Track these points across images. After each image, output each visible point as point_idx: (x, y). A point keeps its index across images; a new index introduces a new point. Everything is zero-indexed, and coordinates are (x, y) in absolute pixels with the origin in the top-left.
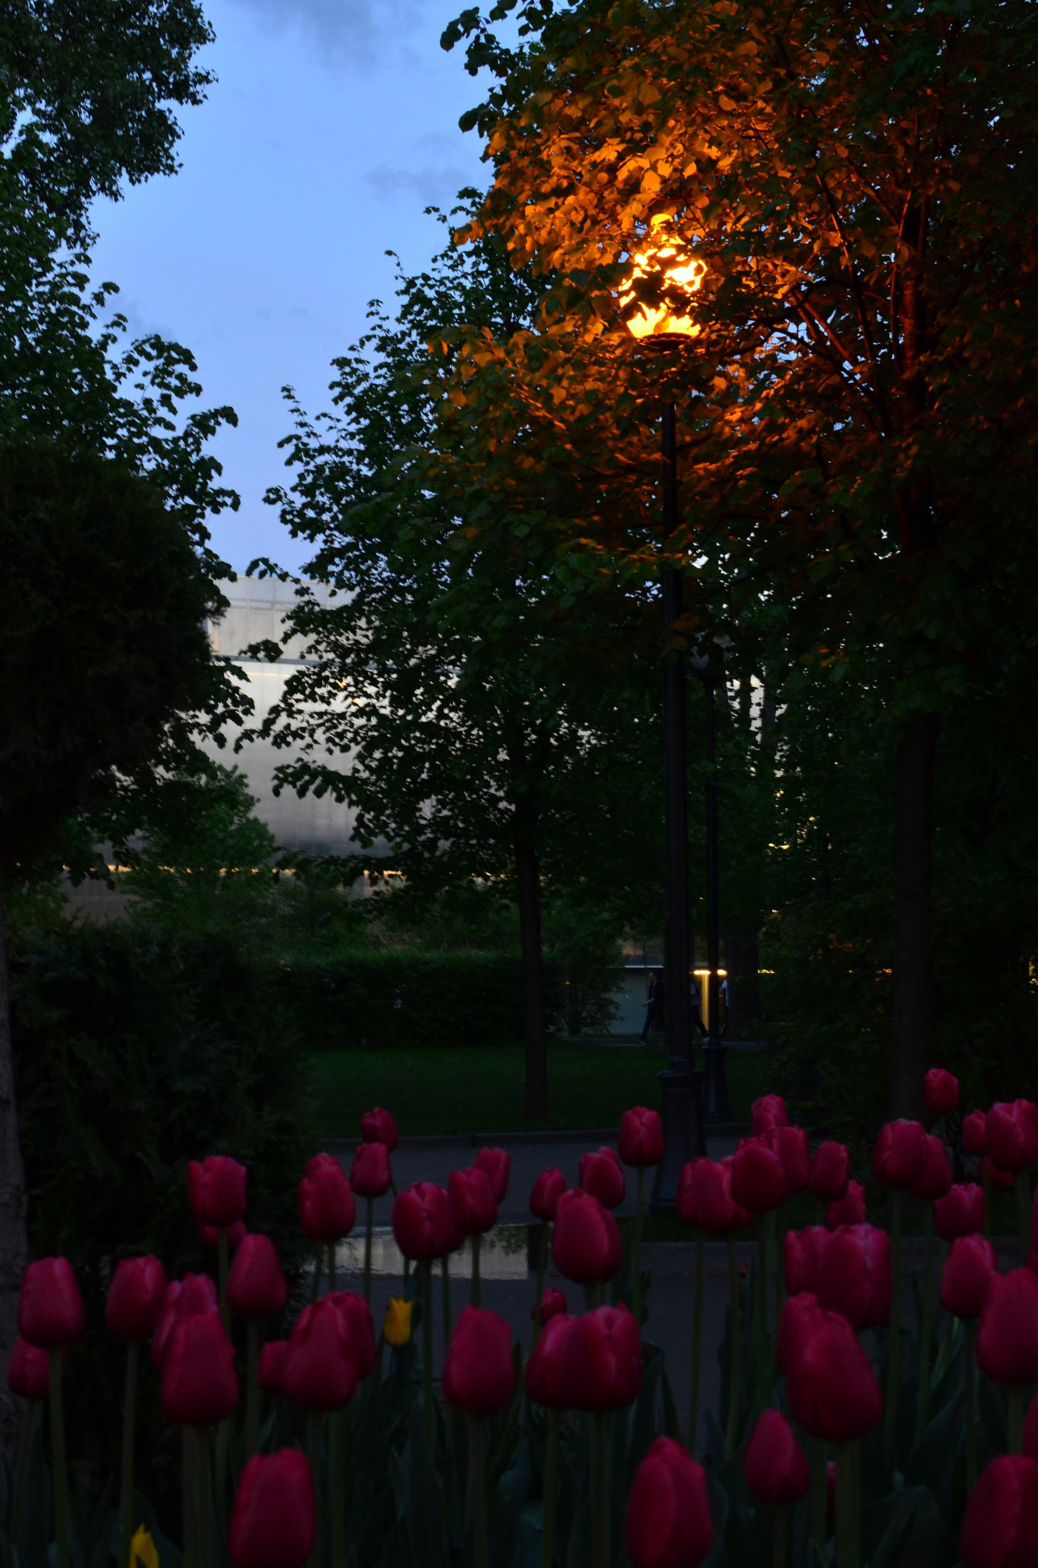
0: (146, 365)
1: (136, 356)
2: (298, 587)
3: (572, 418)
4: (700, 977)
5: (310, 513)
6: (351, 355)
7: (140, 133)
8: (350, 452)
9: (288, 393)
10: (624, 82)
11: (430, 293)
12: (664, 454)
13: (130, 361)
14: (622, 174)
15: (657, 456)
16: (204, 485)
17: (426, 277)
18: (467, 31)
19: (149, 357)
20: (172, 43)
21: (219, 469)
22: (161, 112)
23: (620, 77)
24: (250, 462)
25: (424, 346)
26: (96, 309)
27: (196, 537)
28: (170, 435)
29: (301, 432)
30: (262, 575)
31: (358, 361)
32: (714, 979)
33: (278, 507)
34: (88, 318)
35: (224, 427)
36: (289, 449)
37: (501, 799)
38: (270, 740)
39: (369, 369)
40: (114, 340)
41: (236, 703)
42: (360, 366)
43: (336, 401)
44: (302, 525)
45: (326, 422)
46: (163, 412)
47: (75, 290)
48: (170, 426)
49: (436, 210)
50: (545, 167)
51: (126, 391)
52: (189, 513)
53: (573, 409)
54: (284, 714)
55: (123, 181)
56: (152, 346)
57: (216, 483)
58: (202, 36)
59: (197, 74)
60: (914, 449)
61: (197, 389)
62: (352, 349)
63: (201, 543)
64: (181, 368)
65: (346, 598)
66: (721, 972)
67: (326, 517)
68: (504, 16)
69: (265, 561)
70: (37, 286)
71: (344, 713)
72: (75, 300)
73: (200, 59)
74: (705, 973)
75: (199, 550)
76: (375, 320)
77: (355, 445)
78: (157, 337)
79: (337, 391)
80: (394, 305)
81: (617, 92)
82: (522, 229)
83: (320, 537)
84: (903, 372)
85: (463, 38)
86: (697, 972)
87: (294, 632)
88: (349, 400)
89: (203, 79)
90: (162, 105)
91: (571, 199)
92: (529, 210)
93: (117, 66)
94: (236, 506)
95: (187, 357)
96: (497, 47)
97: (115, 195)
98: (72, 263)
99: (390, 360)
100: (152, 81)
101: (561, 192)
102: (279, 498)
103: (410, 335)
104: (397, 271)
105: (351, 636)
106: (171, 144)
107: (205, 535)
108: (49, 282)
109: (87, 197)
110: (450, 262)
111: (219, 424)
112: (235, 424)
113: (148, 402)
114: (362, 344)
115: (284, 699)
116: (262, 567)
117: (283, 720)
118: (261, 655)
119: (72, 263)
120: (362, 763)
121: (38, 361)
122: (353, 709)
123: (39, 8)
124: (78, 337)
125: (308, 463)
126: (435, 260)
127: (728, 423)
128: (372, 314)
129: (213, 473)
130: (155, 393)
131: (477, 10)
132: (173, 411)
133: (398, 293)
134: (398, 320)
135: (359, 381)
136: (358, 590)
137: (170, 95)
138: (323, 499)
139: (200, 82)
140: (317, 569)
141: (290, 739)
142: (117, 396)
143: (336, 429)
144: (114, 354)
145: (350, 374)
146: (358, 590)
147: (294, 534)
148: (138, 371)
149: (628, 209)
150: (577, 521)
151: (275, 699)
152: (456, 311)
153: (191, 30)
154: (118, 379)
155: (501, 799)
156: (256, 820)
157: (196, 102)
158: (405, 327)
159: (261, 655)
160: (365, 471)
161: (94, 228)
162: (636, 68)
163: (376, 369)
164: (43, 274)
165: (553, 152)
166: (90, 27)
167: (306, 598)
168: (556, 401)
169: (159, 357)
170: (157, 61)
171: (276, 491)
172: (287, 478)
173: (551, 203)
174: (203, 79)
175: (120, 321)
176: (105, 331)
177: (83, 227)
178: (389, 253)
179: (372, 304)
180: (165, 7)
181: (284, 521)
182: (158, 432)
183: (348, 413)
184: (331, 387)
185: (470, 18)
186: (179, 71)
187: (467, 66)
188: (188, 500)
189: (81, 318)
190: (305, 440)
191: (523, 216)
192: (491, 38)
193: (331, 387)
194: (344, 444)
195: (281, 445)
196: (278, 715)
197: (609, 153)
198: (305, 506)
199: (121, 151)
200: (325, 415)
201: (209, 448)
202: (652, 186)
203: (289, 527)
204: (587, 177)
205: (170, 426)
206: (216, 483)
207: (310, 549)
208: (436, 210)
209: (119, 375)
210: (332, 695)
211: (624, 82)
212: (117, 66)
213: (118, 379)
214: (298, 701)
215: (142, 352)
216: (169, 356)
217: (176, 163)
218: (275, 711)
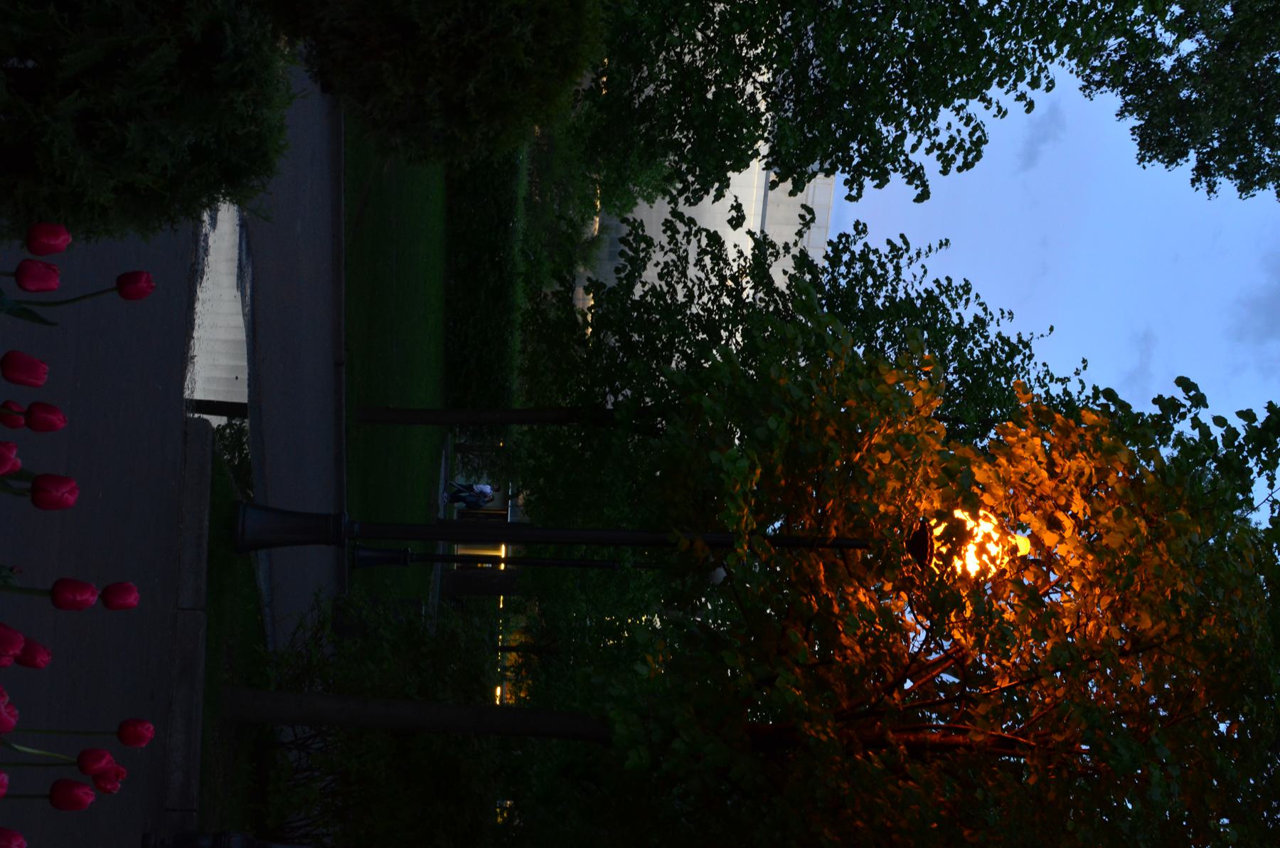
0: (966, 131)
1: (973, 124)
2: (791, 245)
3: (865, 467)
4: (498, 549)
5: (846, 257)
6: (972, 295)
7: (1171, 136)
8: (895, 290)
9: (944, 244)
10: (1125, 521)
11: (1018, 360)
12: (836, 538)
13: (969, 119)
14: (1060, 515)
15: (834, 533)
16: (867, 174)
17: (1031, 357)
18: (1190, 398)
19: (971, 135)
20: (1240, 166)
21: (879, 186)
22: (1187, 154)
23: (1129, 517)
24: (885, 211)
25: (976, 352)
26: (1013, 95)
27: (827, 166)
28: (907, 148)
29: (913, 252)
30: (802, 217)
31: (967, 301)
32: (497, 560)
33: (852, 232)
34: (1006, 87)
35: (913, 192)
36: (899, 243)
37: (616, 398)
38: (669, 217)
39: (961, 309)
40: (987, 108)
41: (695, 192)
42: (963, 302)
43: (937, 281)
44: (838, 247)
45: (920, 273)
46: (926, 143)
47: (1028, 78)
48: (914, 148)
49: (1085, 368)
50: (1070, 455)
51: (945, 115)
52: (847, 161)
53: (872, 468)
54: (687, 229)
55: (1133, 121)
56: (979, 138)
57: (868, 183)
58: (1245, 189)
59: (1215, 183)
60: (824, 738)
61: (945, 172)
62: (977, 296)
63: (821, 169)
64: (960, 160)
65: (781, 282)
66: (502, 566)
67: (843, 269)
68: (1193, 428)
69: (813, 220)
70: (1033, 49)
71: (686, 277)
72: (1021, 77)
73: (1227, 186)
74: (502, 552)
75: (816, 166)
76: (997, 315)
77: (901, 294)
78: (986, 142)
79: (945, 283)
80: (1010, 331)
81: (1118, 515)
82: (1023, 432)
83: (826, 264)
84: (893, 732)
85: (1183, 395)
86: (503, 547)
87: (755, 240)
88: (937, 291)
89: (1211, 188)
90: (1192, 155)
91: (1045, 474)
92: (1037, 441)
93: (1223, 120)
94: (850, 198)
95: (967, 165)
96: (1175, 421)
97: (1121, 114)
98: (1047, 77)
99: (966, 325)
100: (1212, 148)
101: (1051, 465)
102: (858, 233)
103: (986, 342)
104: (1036, 334)
105: (750, 285)
106: (1163, 162)
107: (828, 173)
108: (1035, 58)
109: (1122, 92)
110: (1042, 376)
111: (917, 187)
112: (915, 201)
113: (937, 132)
114: (981, 304)
115: (700, 230)
116: (808, 217)
117: (682, 228)
118: (734, 213)
119: (1047, 77)
120: (650, 290)
121: (973, 46)
122: (690, 284)
123: (1273, 61)
124: (991, 79)
125: (886, 257)
126: (1044, 365)
127: (856, 592)
128: (1003, 313)
129: (877, 182)
130: (943, 138)
131: (1206, 406)
132: (928, 151)
133: (1019, 334)
134: (999, 333)
135: (952, 301)
136: (787, 292)
137: (1199, 161)
138: (858, 268)
139: (1209, 186)
140: (803, 261)
141: (669, 233)
142: (941, 108)
143: (914, 281)
144: (975, 107)
145: (957, 293)
146: (787, 292)
147: (830, 243)
148: (961, 125)
149: (1034, 519)
150: (780, 466)
151: (702, 223)
152: (1003, 380)
153: (1248, 182)
154: (954, 109)
155: (616, 398)
156: (636, 204)
157: (1193, 182)
158: (993, 338)
159: (734, 213)
160: (879, 302)
161: (1097, 96)
162: (1136, 531)
163: (958, 314)
164: (1041, 53)
165: (1081, 463)
166: (1256, 100)
167: (782, 251)
168: (880, 455)
169: (972, 142)
170: (1228, 151)
171: (865, 231)
172: (876, 240)
173: (1041, 459)
174: (1211, 188)
175: (1002, 113)
176: (994, 101)
177: (1099, 88)
178: (1052, 329)
179: (1011, 313)
180: (1268, 160)
181: (840, 236)
182: (911, 139)
183: (926, 290)
184: (948, 278)
185: (1200, 401)
186: (1218, 170)
187: (1160, 397)
188: (856, 160)
189: (1006, 82)
190: (906, 256)
191: (1033, 436)
192: (1183, 416)
193: (948, 278)
194: (901, 286)
195: (902, 236)
196: (686, 225)
197: (1078, 506)
198: (853, 253)
199: (1155, 121)
200: (925, 272)
201: (896, 179)
202: (1049, 538)
203: (835, 240)
204: (1062, 487)
205: (914, 148)
206: (868, 183)
207: (818, 256)
208: (1085, 368)
209: (958, 110)
210: (703, 268)
211: (1125, 521)
212: (1223, 120)
213: (954, 109)
214: (699, 241)
215: (975, 129)
216: (972, 150)
217: (1146, 164)
218: (691, 221)
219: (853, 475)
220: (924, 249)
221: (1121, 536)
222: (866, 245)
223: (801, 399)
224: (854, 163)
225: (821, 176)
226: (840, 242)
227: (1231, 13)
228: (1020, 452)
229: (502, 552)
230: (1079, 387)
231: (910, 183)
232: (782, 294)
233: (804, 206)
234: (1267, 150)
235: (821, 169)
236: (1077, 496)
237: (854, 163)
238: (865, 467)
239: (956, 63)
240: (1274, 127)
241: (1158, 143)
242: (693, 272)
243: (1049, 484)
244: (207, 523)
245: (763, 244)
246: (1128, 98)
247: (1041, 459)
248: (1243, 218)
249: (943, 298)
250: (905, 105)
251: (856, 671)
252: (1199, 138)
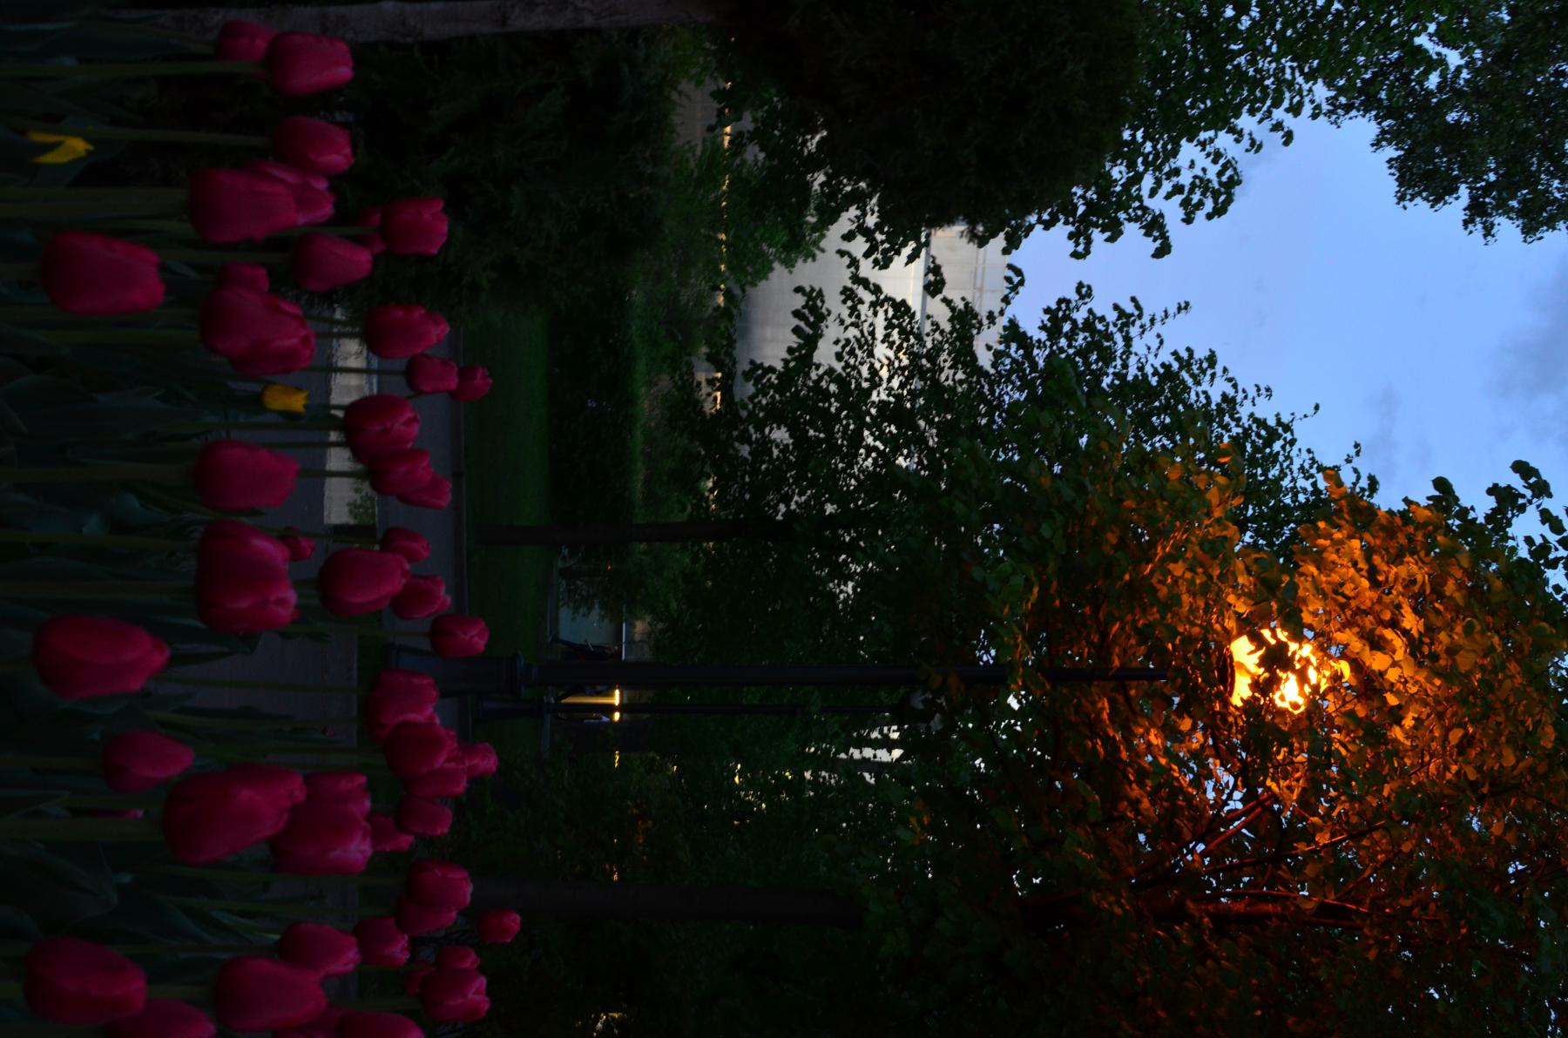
0: (1213, 170)
1: (1222, 161)
3: (1154, 581)
4: (611, 695)
5: (1067, 327)
6: (1219, 369)
7: (1437, 169)
8: (1125, 366)
9: (1184, 307)
10: (1477, 637)
11: (1277, 446)
13: (1217, 156)
15: (1117, 663)
16: (1096, 225)
17: (1293, 442)
18: (1529, 486)
19: (1220, 174)
20: (1523, 202)
21: (1111, 240)
22: (1457, 189)
23: (1483, 633)
24: (1117, 270)
25: (1226, 440)
26: (1267, 124)
27: (1045, 217)
28: (1145, 192)
29: (1146, 320)
30: (1008, 279)
31: (1213, 376)
32: (610, 709)
33: (1073, 296)
34: (1259, 116)
35: (1152, 245)
36: (1129, 308)
37: (788, 506)
38: (849, 284)
39: (1205, 386)
41: (885, 252)
42: (1208, 378)
43: (1175, 353)
44: (1056, 318)
45: (1155, 343)
46: (1167, 186)
47: (1286, 104)
48: (1153, 193)
49: (1358, 454)
50: (1397, 559)
52: (1069, 210)
53: (1163, 582)
54: (873, 298)
55: (1391, 152)
56: (1231, 178)
57: (1098, 236)
58: (1529, 230)
59: (1492, 225)
60: (1119, 911)
61: (1188, 220)
62: (1225, 370)
63: (1040, 221)
64: (1209, 205)
65: (985, 359)
66: (617, 716)
67: (1063, 342)
69: (1022, 283)
72: (1277, 103)
73: (1508, 228)
74: (616, 699)
75: (1033, 219)
76: (1252, 392)
77: (1132, 371)
78: (1239, 182)
79: (1185, 355)
82: (1338, 536)
83: (1043, 336)
85: (1523, 483)
86: (617, 692)
87: (953, 309)
88: (1176, 366)
89: (1488, 231)
90: (1464, 191)
91: (1365, 583)
92: (1356, 543)
94: (1075, 255)
95: (1219, 211)
97: (1377, 144)
98: (1312, 101)
99: (1213, 406)
101: (1372, 574)
102: (1082, 297)
104: (1298, 416)
105: (948, 364)
106: (1426, 199)
107: (1048, 225)
109: (1376, 117)
110: (1307, 466)
112: (1154, 256)
113: (1177, 172)
114: (1230, 380)
115: (887, 299)
116: (1016, 279)
117: (868, 297)
118: (931, 277)
119: (1312, 101)
120: (825, 373)
121: (1219, 67)
122: (877, 365)
126: (1309, 451)
127: (1147, 732)
129: (1108, 234)
130: (1185, 179)
131: (1550, 496)
132: (1168, 197)
134: (1252, 415)
135: (1193, 376)
136: (992, 371)
137: (1473, 198)
138: (1080, 339)
139: (1485, 228)
140: (1013, 333)
141: (849, 303)
142: (1183, 142)
143: (1148, 353)
144: (1224, 140)
145: (1200, 368)
146: (992, 371)
147: (1047, 311)
148: (1207, 163)
150: (1055, 584)
153: (1534, 220)
155: (788, 506)
157: (1466, 223)
158: (1245, 422)
159: (931, 277)
160: (1106, 381)
161: (1346, 122)
162: (1492, 648)
163: (1205, 392)
164: (1302, 73)
165: (1411, 567)
166: (1539, 123)
167: (985, 322)
168: (1171, 566)
169: (1220, 183)
170: (1506, 187)
171: (1089, 295)
172: (1101, 305)
174: (1488, 231)
175: (1256, 146)
176: (1246, 132)
178: (1317, 407)
179: (1268, 390)
180: (1558, 195)
181: (1060, 301)
182: (1148, 182)
183: (1163, 365)
184: (1189, 350)
186: (1496, 208)
187: (1496, 485)
188: (1081, 209)
189: (1259, 109)
190: (1138, 323)
191: (1350, 537)
192: (1522, 509)
193: (1189, 350)
194: (1133, 360)
195: (1133, 299)
197: (1410, 621)
198: (1074, 322)
199: (1419, 150)
200: (1161, 342)
201: (1132, 231)
202: (1377, 661)
203: (1054, 306)
204: (1387, 599)
205: (1153, 193)
206: (1098, 236)
207: (1032, 326)
208: (1358, 454)
209: (1203, 144)
211: (1477, 637)
215: (1225, 167)
216: (1220, 194)
217: (1407, 203)
218: (877, 290)
219: (1138, 593)
220: (1159, 315)
221: (1473, 655)
222: (1090, 311)
223: (1074, 501)
224: (1080, 212)
225: (1039, 227)
226: (1059, 309)
227: (1507, 18)
228: (1334, 557)
229: (616, 699)
230: (1353, 478)
231: (1147, 234)
232: (986, 374)
233: (1010, 267)
234: (1556, 183)
235: (1040, 221)
236: (1407, 610)
237: (1080, 212)
238: (1154, 581)
239: (1213, 93)
240: (1564, 154)
241: (1421, 177)
242: (881, 351)
243: (1369, 595)
244: (355, 673)
245: (965, 319)
246: (1385, 124)
247: (1361, 565)
248: (1515, 264)
249: (1184, 374)
250: (1139, 139)
251: (127, 878)
252: (1473, 171)
